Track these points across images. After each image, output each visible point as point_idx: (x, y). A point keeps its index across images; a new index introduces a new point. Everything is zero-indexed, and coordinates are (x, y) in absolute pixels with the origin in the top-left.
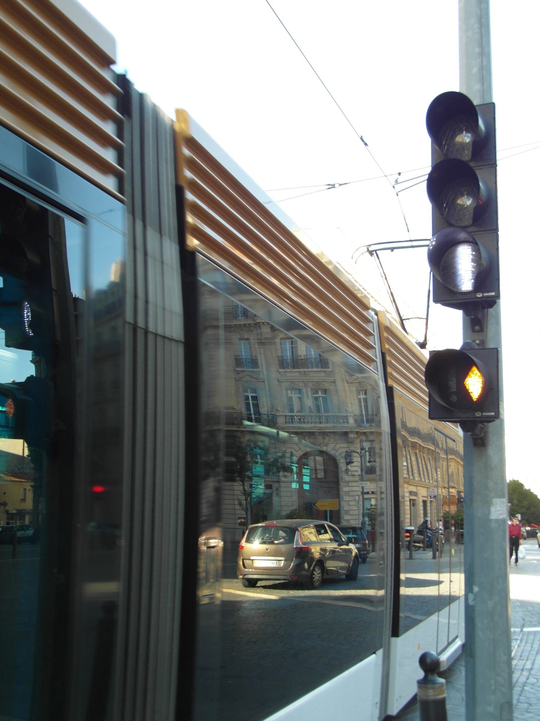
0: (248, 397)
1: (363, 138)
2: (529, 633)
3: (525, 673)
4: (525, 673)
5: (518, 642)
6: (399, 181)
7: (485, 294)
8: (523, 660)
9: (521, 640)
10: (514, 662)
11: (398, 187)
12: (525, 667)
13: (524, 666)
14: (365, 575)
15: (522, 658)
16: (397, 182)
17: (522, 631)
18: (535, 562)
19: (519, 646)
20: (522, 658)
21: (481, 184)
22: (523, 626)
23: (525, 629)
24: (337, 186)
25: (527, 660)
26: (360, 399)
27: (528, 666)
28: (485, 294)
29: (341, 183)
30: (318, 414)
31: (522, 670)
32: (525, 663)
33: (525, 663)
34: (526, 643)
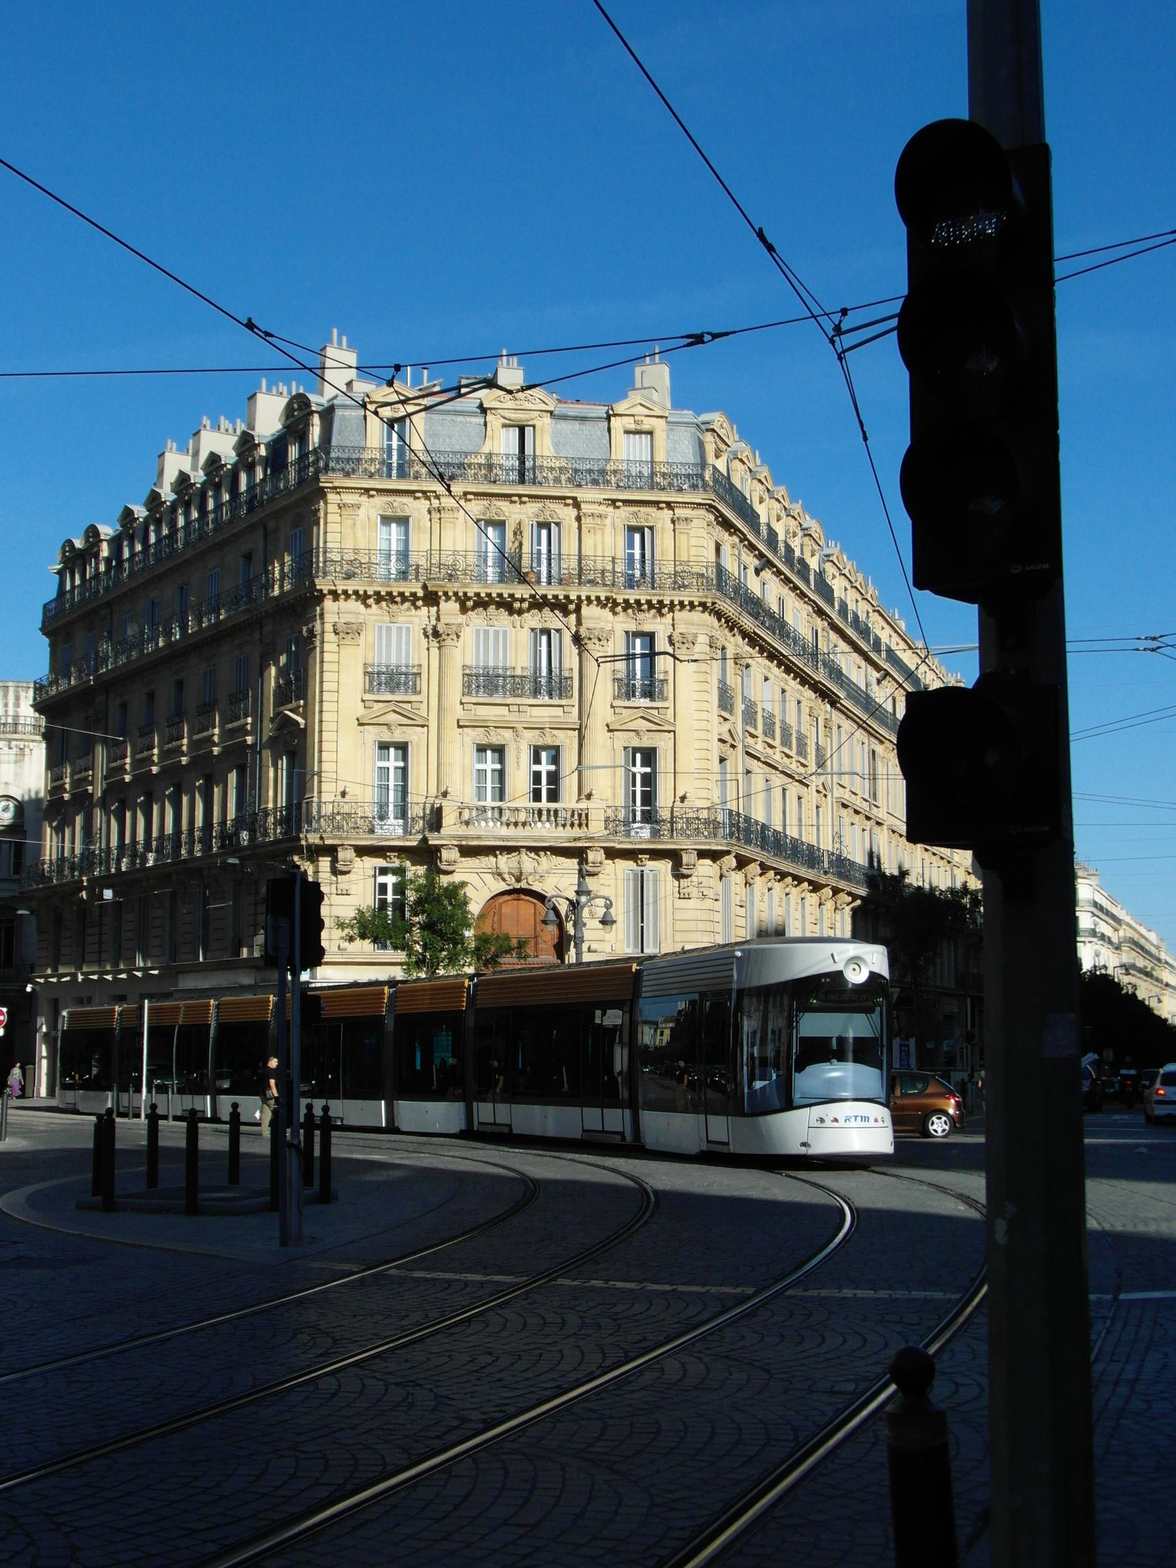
0: (550, 800)
1: (765, 233)
2: (1132, 1302)
3: (1123, 1390)
4: (1123, 1390)
5: (1109, 1322)
6: (844, 327)
7: (1028, 568)
8: (1117, 1361)
9: (1113, 1320)
10: (1098, 1368)
11: (848, 340)
12: (1122, 1377)
13: (1120, 1374)
14: (1160, 1144)
15: (1115, 1358)
16: (840, 328)
17: (1116, 1299)
18: (1144, 1150)
19: (1108, 1332)
20: (1115, 1358)
21: (1017, 325)
22: (1118, 1289)
23: (1122, 1296)
24: (707, 338)
25: (1127, 1362)
26: (634, 775)
27: (1129, 1375)
28: (1028, 568)
29: (715, 331)
30: (498, 804)
31: (1116, 1383)
32: (1123, 1369)
33: (1123, 1369)
34: (1124, 1326)
